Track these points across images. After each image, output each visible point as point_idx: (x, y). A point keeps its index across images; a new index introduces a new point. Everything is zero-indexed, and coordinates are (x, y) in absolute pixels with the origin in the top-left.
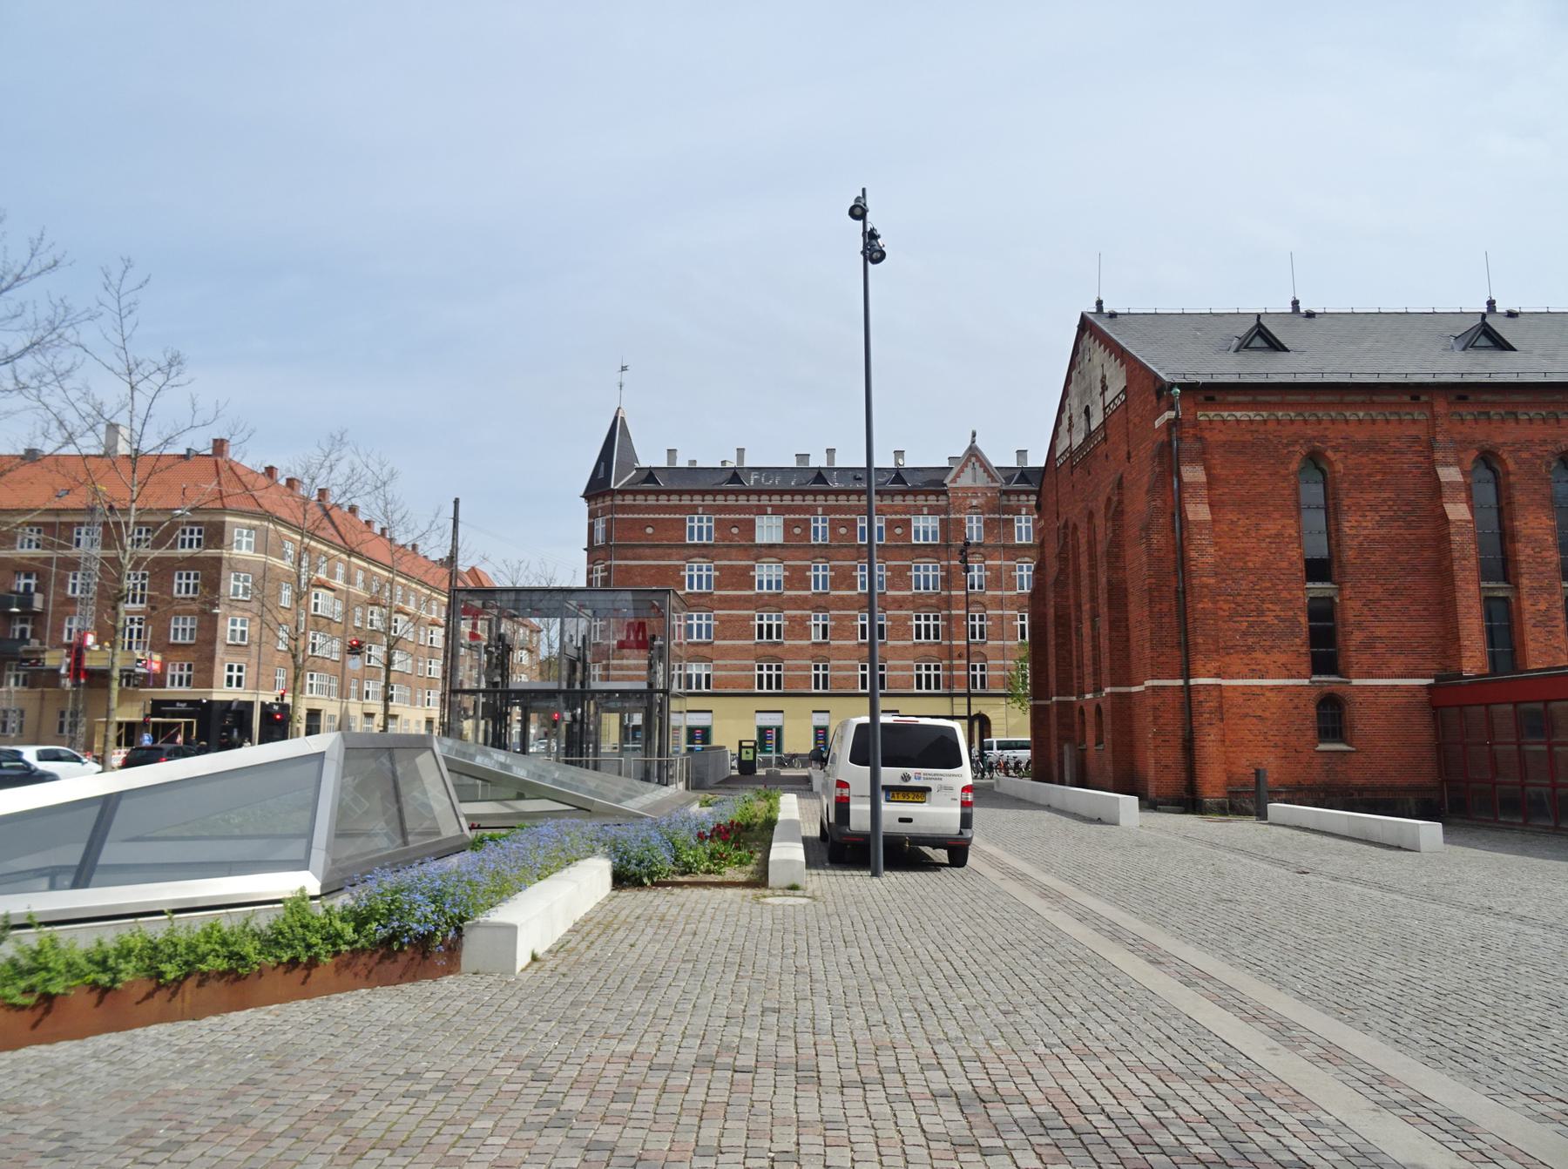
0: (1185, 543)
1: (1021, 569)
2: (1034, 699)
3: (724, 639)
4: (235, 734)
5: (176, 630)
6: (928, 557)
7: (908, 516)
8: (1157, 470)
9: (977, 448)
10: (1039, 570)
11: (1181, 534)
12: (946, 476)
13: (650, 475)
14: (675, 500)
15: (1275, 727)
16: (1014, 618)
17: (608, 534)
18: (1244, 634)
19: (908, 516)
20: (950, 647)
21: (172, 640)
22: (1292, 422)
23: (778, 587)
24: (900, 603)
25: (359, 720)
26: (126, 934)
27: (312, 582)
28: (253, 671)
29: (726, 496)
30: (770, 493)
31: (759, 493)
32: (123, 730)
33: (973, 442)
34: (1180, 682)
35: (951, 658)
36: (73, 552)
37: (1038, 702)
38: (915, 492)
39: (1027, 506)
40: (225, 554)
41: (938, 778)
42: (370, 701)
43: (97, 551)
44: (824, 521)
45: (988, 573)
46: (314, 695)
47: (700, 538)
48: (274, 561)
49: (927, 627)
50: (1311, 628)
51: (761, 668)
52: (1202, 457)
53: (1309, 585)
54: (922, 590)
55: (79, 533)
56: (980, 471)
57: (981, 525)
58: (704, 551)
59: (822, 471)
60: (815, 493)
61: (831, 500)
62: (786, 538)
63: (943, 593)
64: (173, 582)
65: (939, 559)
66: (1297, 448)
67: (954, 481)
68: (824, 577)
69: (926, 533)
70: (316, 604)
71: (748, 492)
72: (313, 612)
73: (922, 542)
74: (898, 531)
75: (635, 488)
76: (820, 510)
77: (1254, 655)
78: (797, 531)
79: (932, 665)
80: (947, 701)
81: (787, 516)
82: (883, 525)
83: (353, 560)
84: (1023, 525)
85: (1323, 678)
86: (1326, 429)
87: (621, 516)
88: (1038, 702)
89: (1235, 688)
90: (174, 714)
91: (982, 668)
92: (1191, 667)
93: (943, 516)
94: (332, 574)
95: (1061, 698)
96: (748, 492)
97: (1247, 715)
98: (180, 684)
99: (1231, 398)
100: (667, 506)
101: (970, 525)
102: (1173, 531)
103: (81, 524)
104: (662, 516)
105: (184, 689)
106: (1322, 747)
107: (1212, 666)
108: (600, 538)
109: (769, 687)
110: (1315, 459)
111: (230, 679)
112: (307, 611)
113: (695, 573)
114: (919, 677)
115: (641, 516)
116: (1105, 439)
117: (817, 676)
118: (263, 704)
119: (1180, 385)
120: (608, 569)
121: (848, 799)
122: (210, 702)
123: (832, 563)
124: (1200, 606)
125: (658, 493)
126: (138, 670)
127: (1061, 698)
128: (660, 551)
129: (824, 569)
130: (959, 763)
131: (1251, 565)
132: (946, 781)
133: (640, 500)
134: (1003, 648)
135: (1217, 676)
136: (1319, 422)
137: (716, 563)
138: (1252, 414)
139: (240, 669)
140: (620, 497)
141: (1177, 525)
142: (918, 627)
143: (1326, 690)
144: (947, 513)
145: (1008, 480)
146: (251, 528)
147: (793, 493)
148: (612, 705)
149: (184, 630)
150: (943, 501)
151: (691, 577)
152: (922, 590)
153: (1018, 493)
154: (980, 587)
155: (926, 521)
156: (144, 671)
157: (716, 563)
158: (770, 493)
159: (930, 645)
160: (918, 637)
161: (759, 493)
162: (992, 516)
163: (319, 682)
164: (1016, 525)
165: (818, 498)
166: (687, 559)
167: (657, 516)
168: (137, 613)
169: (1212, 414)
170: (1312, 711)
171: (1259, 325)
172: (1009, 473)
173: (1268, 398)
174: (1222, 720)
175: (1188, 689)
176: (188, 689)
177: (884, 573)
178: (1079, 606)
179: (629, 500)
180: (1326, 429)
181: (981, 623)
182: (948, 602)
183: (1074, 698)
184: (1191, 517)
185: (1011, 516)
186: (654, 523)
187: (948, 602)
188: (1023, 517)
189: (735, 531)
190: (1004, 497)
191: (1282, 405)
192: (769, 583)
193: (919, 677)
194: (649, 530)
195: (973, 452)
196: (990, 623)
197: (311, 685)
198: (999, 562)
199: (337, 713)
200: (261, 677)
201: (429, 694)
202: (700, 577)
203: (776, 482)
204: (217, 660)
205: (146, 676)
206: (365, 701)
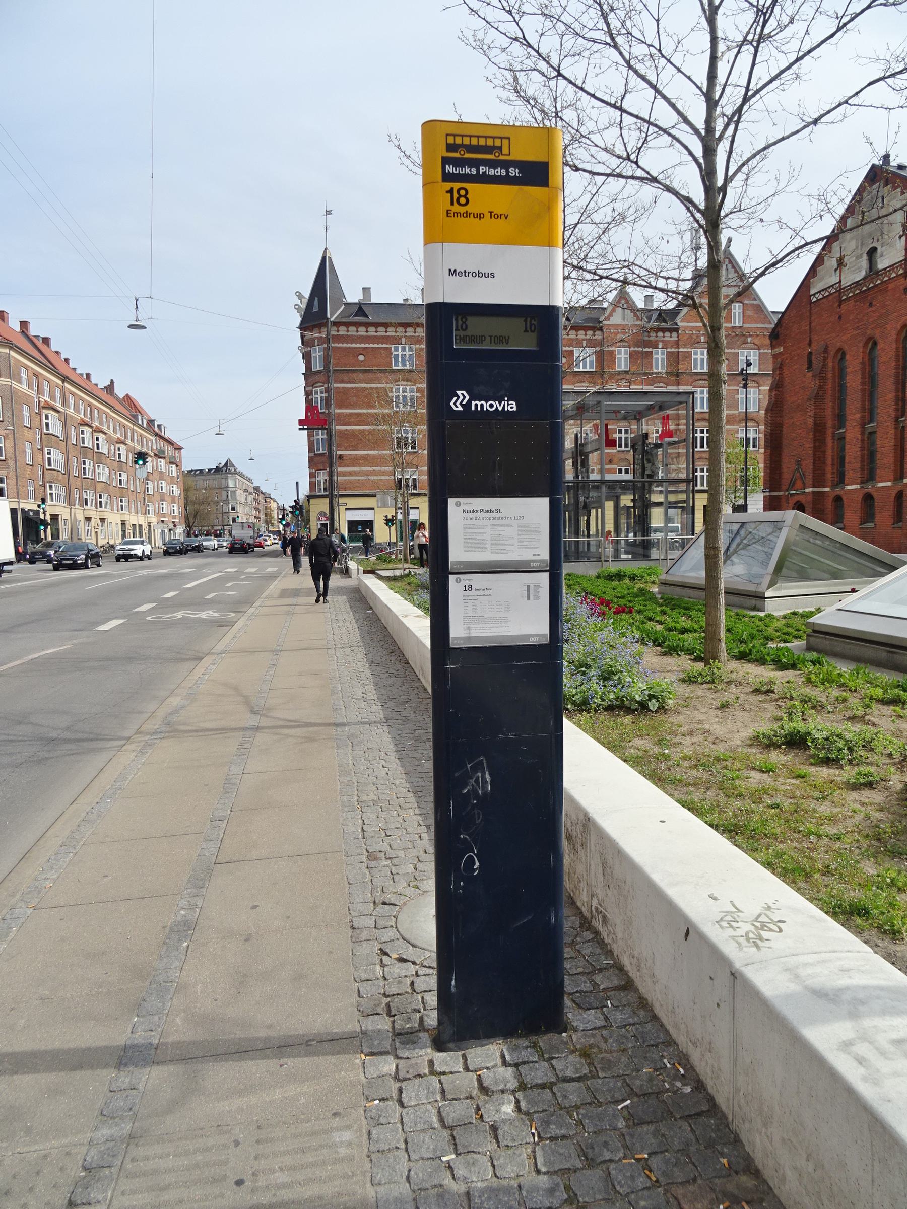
7: (571, 348)
14: (381, 331)
17: (326, 360)
19: (571, 348)
25: (82, 522)
27: (42, 405)
29: (376, 328)
39: (662, 341)
42: (89, 507)
48: (15, 385)
59: (364, 308)
67: (607, 319)
70: (47, 425)
72: (45, 431)
75: (347, 320)
83: (66, 385)
87: (336, 345)
94: (52, 397)
95: (816, 490)
100: (375, 337)
101: (619, 356)
104: (371, 345)
108: (317, 366)
112: (41, 430)
115: (354, 345)
120: (328, 391)
125: (367, 325)
127: (816, 490)
128: (371, 376)
133: (352, 331)
137: (418, 386)
140: (335, 328)
150: (598, 336)
162: (636, 349)
163: (57, 492)
164: (654, 356)
165: (388, 330)
167: (367, 345)
179: (343, 331)
181: (627, 435)
185: (650, 349)
186: (363, 352)
188: (660, 350)
194: (361, 358)
197: (51, 494)
200: (20, 488)
201: (122, 501)
206: (86, 507)
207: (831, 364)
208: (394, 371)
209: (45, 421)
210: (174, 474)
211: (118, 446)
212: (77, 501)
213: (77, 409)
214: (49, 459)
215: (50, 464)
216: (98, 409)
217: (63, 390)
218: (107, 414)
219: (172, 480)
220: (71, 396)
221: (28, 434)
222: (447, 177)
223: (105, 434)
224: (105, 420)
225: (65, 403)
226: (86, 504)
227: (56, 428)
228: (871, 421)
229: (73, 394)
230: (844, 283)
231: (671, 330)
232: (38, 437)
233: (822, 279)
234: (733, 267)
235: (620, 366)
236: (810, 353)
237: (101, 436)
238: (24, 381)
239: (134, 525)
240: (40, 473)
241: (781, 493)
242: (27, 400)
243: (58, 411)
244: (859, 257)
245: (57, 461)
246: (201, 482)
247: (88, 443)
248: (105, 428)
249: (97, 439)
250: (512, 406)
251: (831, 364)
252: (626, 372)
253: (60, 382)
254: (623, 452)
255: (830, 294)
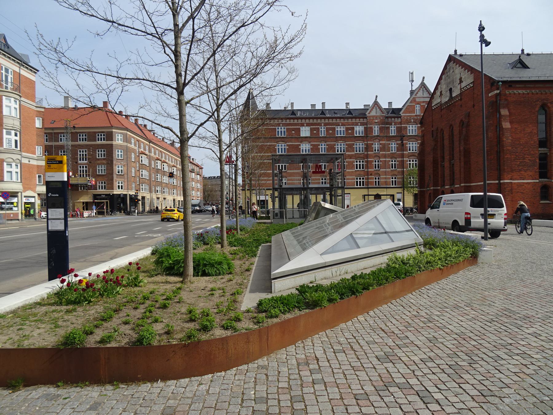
0: (501, 136)
1: (392, 144)
2: (112, 145)
3: (291, 170)
4: (122, 205)
5: (99, 170)
6: (360, 140)
8: (491, 111)
9: (377, 102)
10: (422, 145)
11: (499, 133)
12: (367, 111)
13: (263, 111)
15: (527, 196)
16: (389, 161)
18: (519, 166)
20: (368, 171)
21: (98, 173)
22: (537, 93)
23: (309, 152)
24: (350, 157)
26: (390, 256)
28: (126, 184)
30: (305, 118)
31: (302, 118)
32: (85, 205)
33: (376, 99)
34: (497, 182)
35: (368, 175)
36: (60, 143)
37: (421, 189)
38: (355, 118)
39: (394, 122)
40: (114, 143)
41: (498, 211)
42: (158, 193)
43: (70, 143)
44: (324, 128)
45: (381, 146)
46: (143, 192)
47: (281, 135)
48: (129, 145)
49: (360, 165)
50: (540, 164)
51: (357, 179)
52: (507, 106)
53: (540, 149)
54: (411, 151)
55: (61, 136)
56: (378, 110)
57: (378, 129)
58: (283, 140)
60: (321, 118)
61: (327, 121)
62: (311, 135)
63: (365, 153)
64: (96, 153)
65: (364, 141)
66: (538, 103)
67: (369, 113)
68: (325, 148)
69: (359, 132)
70: (142, 160)
71: (298, 119)
73: (358, 135)
74: (350, 131)
76: (323, 124)
77: (521, 172)
78: (315, 132)
79: (362, 178)
80: (366, 190)
81: (311, 127)
82: (345, 129)
83: (151, 144)
84: (393, 129)
85: (543, 180)
86: (548, 96)
88: (421, 189)
89: (515, 183)
90: (101, 199)
91: (378, 179)
92: (501, 176)
93: (365, 126)
94: (145, 149)
95: (435, 188)
96: (298, 119)
97: (518, 192)
98: (102, 189)
99: (518, 86)
102: (497, 131)
103: (63, 133)
105: (103, 190)
106: (542, 202)
107: (510, 176)
109: (360, 185)
110: (544, 107)
111: (119, 186)
112: (139, 162)
113: (280, 147)
114: (357, 182)
116: (461, 100)
117: (392, 181)
118: (130, 195)
119: (502, 81)
121: (470, 218)
122: (113, 195)
123: (327, 143)
124: (506, 156)
126: (89, 184)
127: (435, 188)
129: (324, 145)
130: (503, 207)
131: (521, 142)
132: (500, 212)
134: (386, 172)
135: (511, 179)
136: (546, 93)
137: (287, 143)
138: (524, 91)
139: (122, 183)
141: (498, 129)
142: (357, 165)
143: (544, 183)
144: (367, 125)
145: (388, 113)
146: (121, 133)
147: (313, 118)
148: (313, 192)
149: (102, 170)
150: (365, 121)
151: (279, 149)
152: (411, 151)
153: (391, 117)
154: (378, 150)
155: (359, 128)
156: (90, 184)
157: (287, 143)
158: (305, 118)
159: (361, 171)
160: (357, 168)
161: (302, 118)
164: (391, 129)
166: (277, 142)
168: (85, 164)
169: (511, 91)
170: (539, 190)
171: (520, 59)
172: (389, 110)
173: (529, 86)
174: (512, 194)
175: (500, 183)
176: (105, 190)
177: (345, 146)
178: (443, 157)
180: (548, 96)
182: (367, 156)
183: (439, 188)
184: (504, 127)
187: (367, 156)
189: (293, 132)
190: (387, 119)
191: (534, 88)
192: (306, 150)
193: (357, 182)
195: (376, 103)
196: (381, 163)
197: (142, 188)
198: (384, 142)
199: (149, 198)
200: (129, 186)
202: (282, 149)
203: (307, 115)
204: (114, 180)
205: (91, 186)
207: (439, 136)
208: (277, 138)
209: (141, 159)
210: (199, 179)
211: (173, 168)
212: (153, 191)
213: (155, 154)
214: (142, 174)
215: (142, 176)
216: (165, 153)
217: (149, 146)
218: (168, 155)
219: (197, 181)
220: (153, 149)
221: (133, 164)
222: (48, 163)
223: (167, 163)
224: (167, 157)
225: (150, 151)
226: (157, 192)
227: (145, 161)
228: (453, 159)
229: (154, 148)
230: (443, 102)
231: (398, 117)
232: (138, 165)
233: (435, 100)
234: (426, 89)
235: (375, 133)
236: (433, 130)
237: (165, 164)
238: (133, 143)
239: (179, 201)
240: (138, 180)
241: (425, 189)
242: (134, 151)
243: (146, 155)
244: (447, 91)
245: (145, 175)
246: (209, 182)
247: (159, 167)
248: (167, 161)
249: (164, 165)
250: (58, 195)
251: (439, 136)
252: (378, 136)
253: (148, 143)
254: (377, 170)
255: (438, 106)
